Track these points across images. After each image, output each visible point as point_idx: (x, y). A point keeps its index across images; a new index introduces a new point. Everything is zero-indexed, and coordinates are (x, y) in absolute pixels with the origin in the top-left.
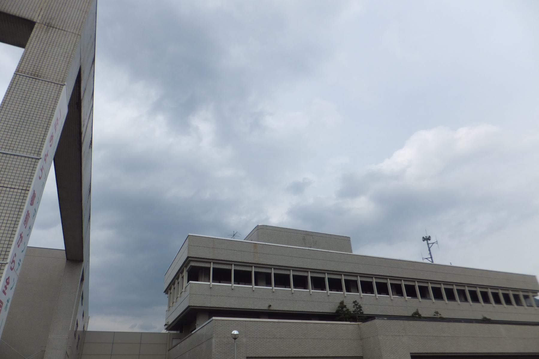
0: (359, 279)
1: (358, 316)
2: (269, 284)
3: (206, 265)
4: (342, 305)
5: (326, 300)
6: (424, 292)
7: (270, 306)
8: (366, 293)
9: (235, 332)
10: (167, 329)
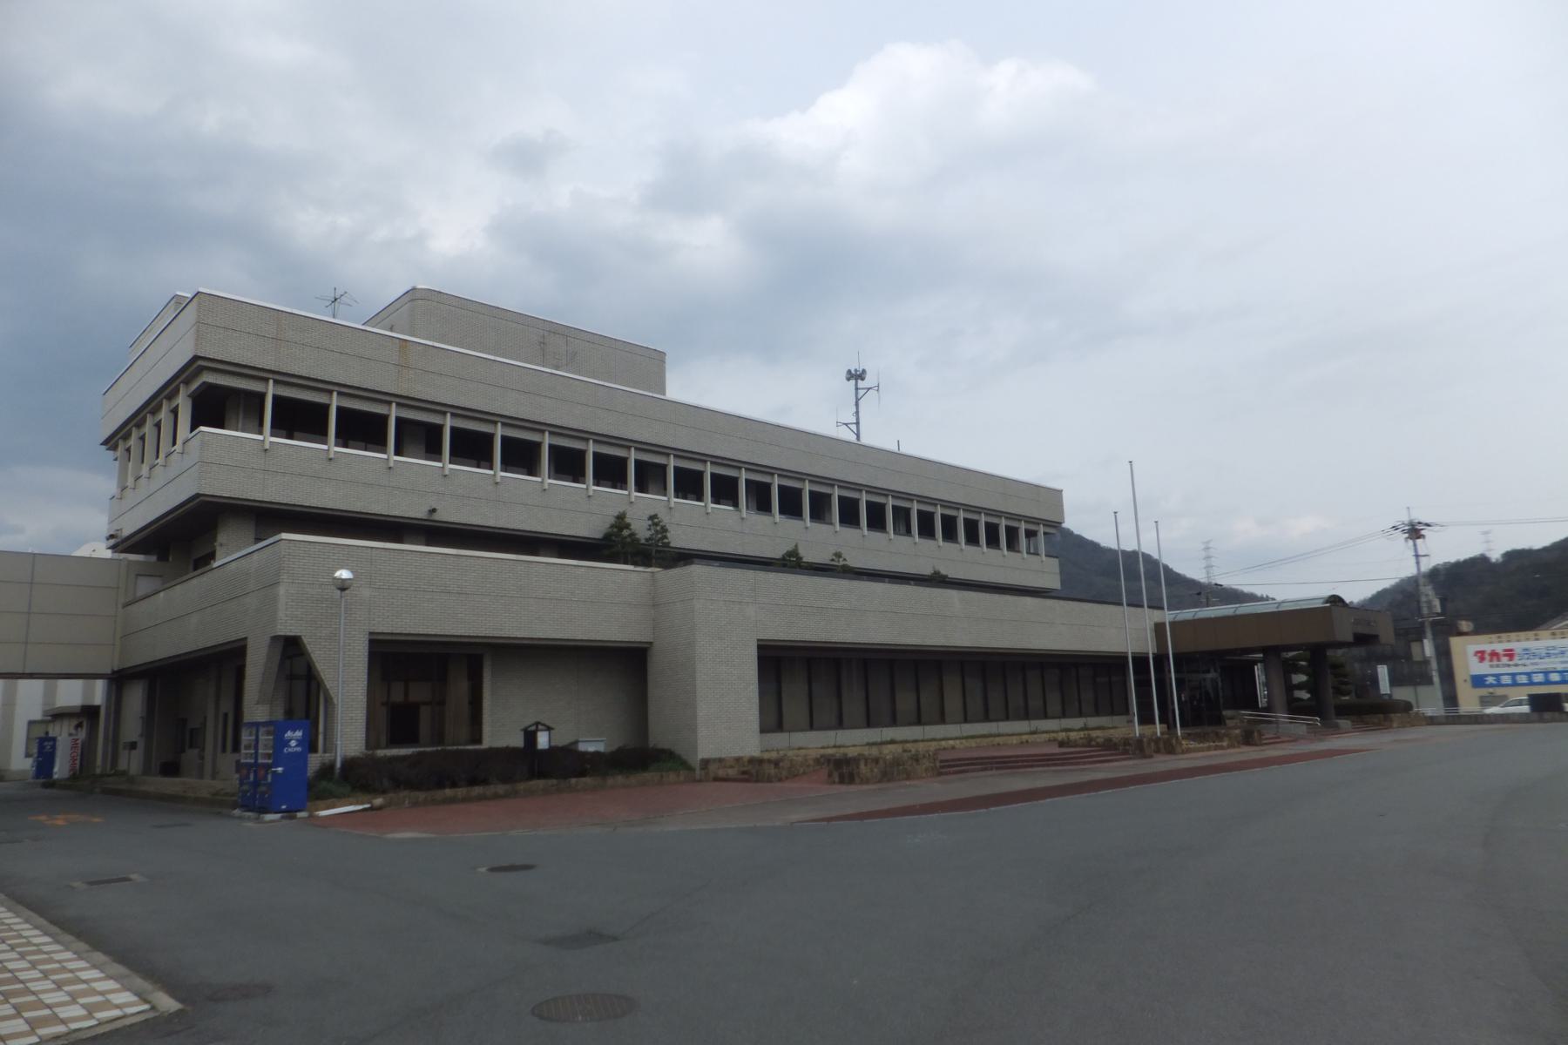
1: (654, 552)
2: (433, 451)
3: (255, 386)
4: (621, 522)
5: (584, 507)
7: (433, 511)
8: (685, 498)
9: (344, 574)
10: (113, 548)
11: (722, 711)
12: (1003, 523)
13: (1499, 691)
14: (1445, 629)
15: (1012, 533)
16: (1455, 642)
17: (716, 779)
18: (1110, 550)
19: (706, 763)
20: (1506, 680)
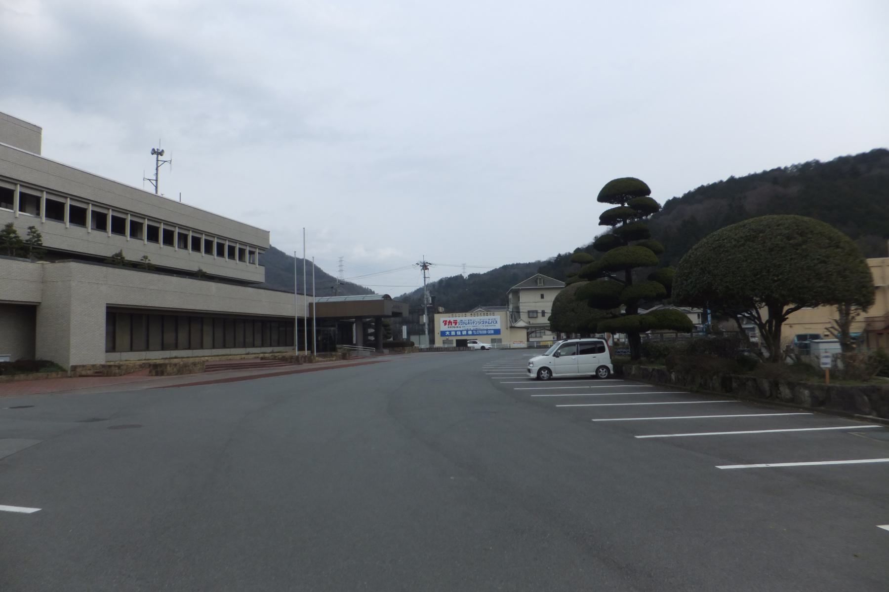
0: (44, 196)
6: (136, 230)
11: (84, 339)
12: (238, 246)
13: (450, 338)
14: (433, 311)
15: (242, 252)
16: (436, 316)
17: (81, 376)
18: (291, 257)
19: (74, 368)
20: (453, 333)
